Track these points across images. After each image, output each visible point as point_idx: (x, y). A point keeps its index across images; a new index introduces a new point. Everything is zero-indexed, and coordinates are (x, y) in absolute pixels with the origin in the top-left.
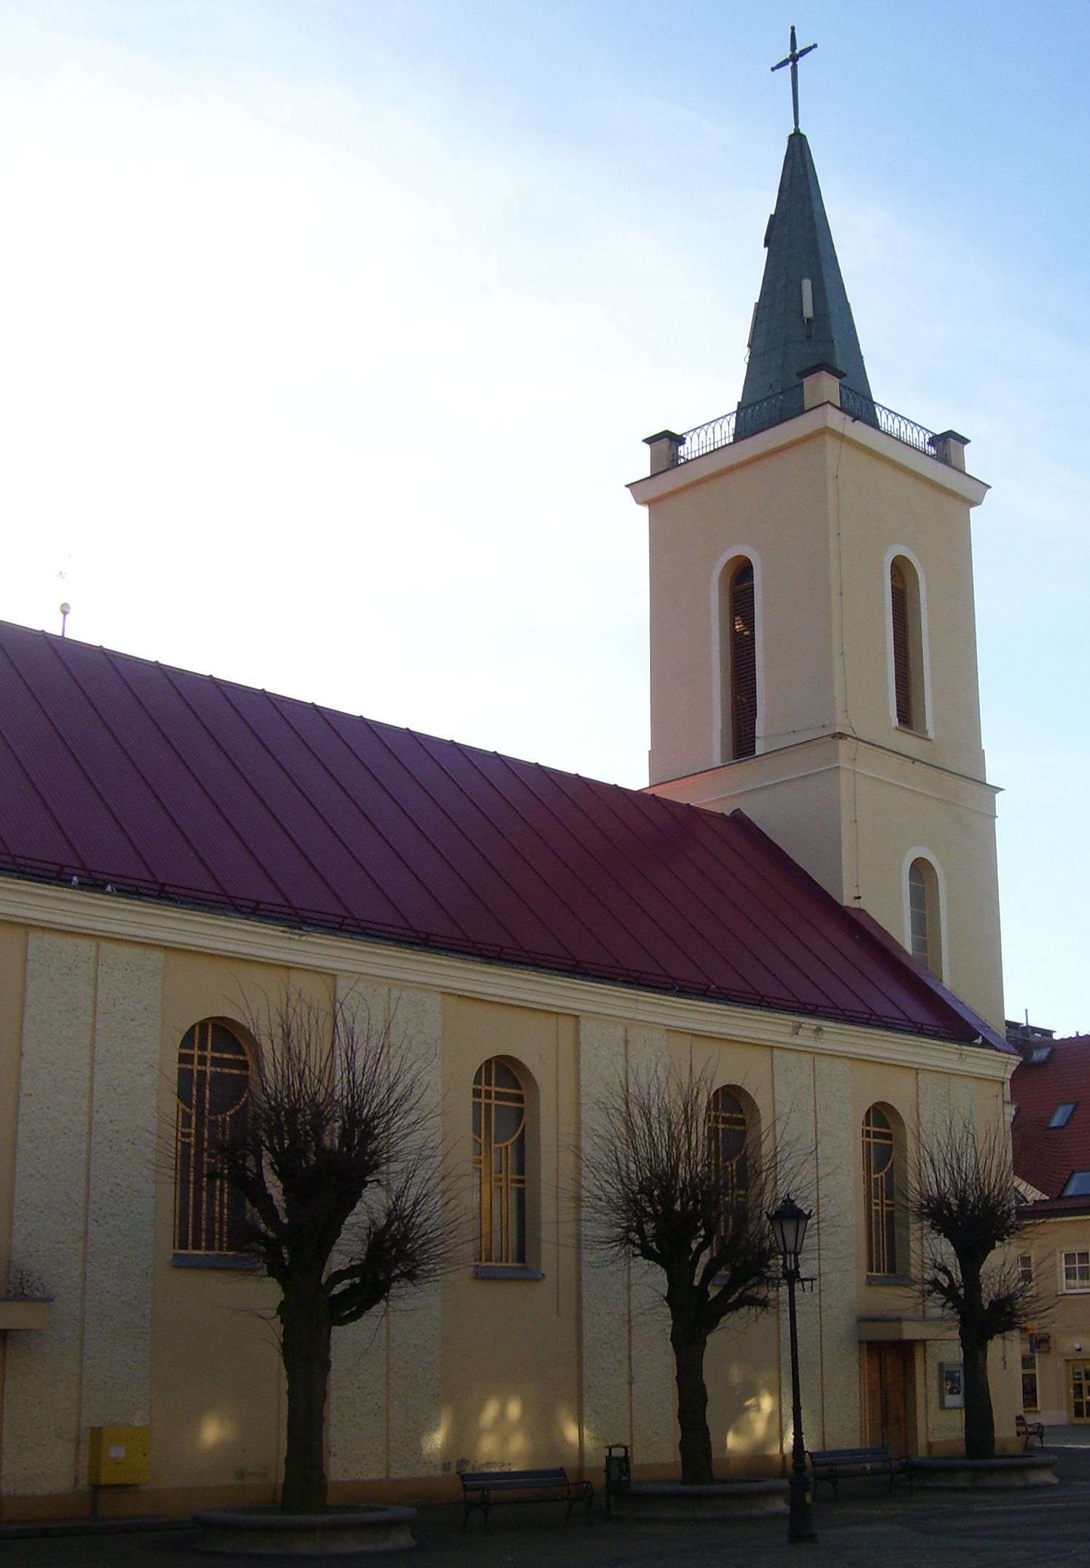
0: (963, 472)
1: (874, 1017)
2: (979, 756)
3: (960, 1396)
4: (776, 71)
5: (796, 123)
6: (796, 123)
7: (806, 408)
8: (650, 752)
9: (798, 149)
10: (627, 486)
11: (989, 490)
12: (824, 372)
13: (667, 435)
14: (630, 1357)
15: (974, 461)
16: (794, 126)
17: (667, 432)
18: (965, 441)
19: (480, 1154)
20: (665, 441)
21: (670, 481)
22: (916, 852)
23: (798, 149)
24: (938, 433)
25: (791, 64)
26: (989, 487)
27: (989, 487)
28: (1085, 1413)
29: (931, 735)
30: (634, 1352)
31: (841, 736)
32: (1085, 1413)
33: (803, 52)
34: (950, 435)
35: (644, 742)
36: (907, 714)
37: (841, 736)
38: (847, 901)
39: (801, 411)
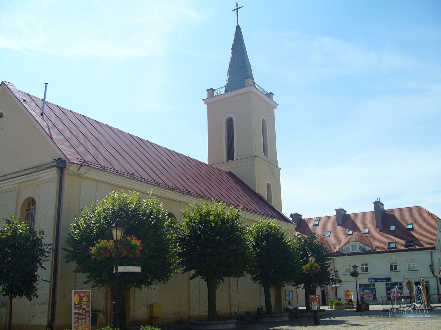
0: (273, 100)
1: (264, 214)
2: (277, 161)
3: (432, 297)
4: (233, 11)
5: (238, 23)
6: (238, 23)
7: (246, 86)
8: (208, 158)
9: (238, 28)
10: (203, 100)
11: (278, 106)
12: (250, 78)
13: (212, 89)
14: (238, 288)
15: (275, 99)
16: (237, 24)
17: (212, 88)
18: (273, 95)
19: (410, 261)
20: (211, 90)
21: (213, 100)
22: (268, 181)
23: (238, 28)
24: (269, 92)
25: (236, 10)
26: (278, 105)
27: (278, 105)
28: (375, 296)
29: (269, 157)
30: (238, 287)
31: (255, 156)
32: (375, 296)
33: (239, 8)
34: (271, 93)
35: (207, 156)
36: (265, 152)
37: (255, 156)
38: (257, 192)
39: (245, 87)
